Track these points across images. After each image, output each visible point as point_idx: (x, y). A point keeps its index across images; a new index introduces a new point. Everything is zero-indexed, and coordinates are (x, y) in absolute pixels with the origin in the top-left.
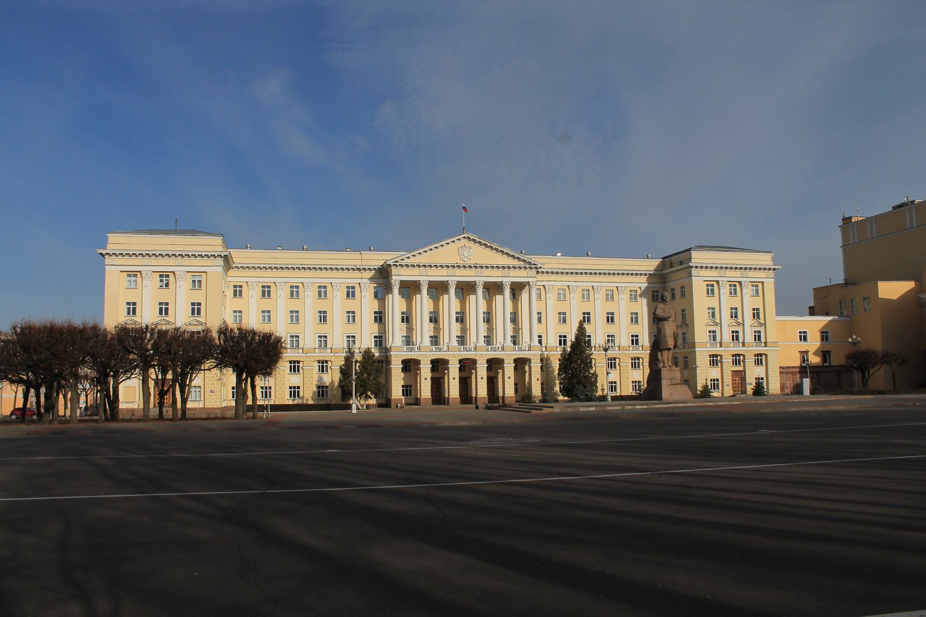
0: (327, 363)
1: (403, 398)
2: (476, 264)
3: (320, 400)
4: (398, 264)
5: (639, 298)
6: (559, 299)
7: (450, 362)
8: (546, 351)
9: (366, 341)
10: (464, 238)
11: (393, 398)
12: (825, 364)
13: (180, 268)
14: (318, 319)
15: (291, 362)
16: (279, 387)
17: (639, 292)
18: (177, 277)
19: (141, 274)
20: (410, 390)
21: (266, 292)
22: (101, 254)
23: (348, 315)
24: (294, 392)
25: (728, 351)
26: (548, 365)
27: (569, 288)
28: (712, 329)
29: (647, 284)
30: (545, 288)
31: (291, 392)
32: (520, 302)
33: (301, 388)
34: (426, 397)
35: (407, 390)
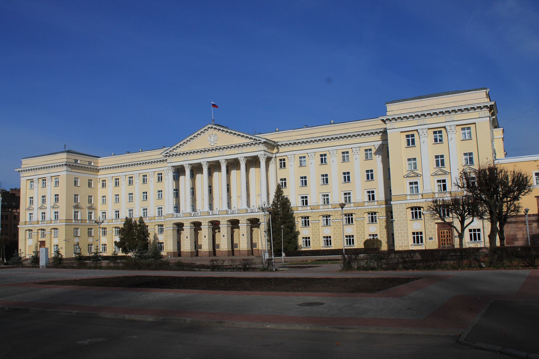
0: (352, 216)
2: (217, 147)
3: (415, 245)
5: (373, 155)
6: (300, 165)
7: (203, 224)
9: (137, 215)
13: (136, 172)
14: (343, 179)
15: (159, 226)
16: (338, 237)
17: (374, 151)
18: (448, 131)
19: (418, 132)
20: (353, 240)
21: (323, 159)
22: (382, 120)
23: (323, 177)
24: (475, 234)
25: (35, 228)
28: (441, 178)
29: (381, 142)
31: (471, 235)
33: (423, 233)
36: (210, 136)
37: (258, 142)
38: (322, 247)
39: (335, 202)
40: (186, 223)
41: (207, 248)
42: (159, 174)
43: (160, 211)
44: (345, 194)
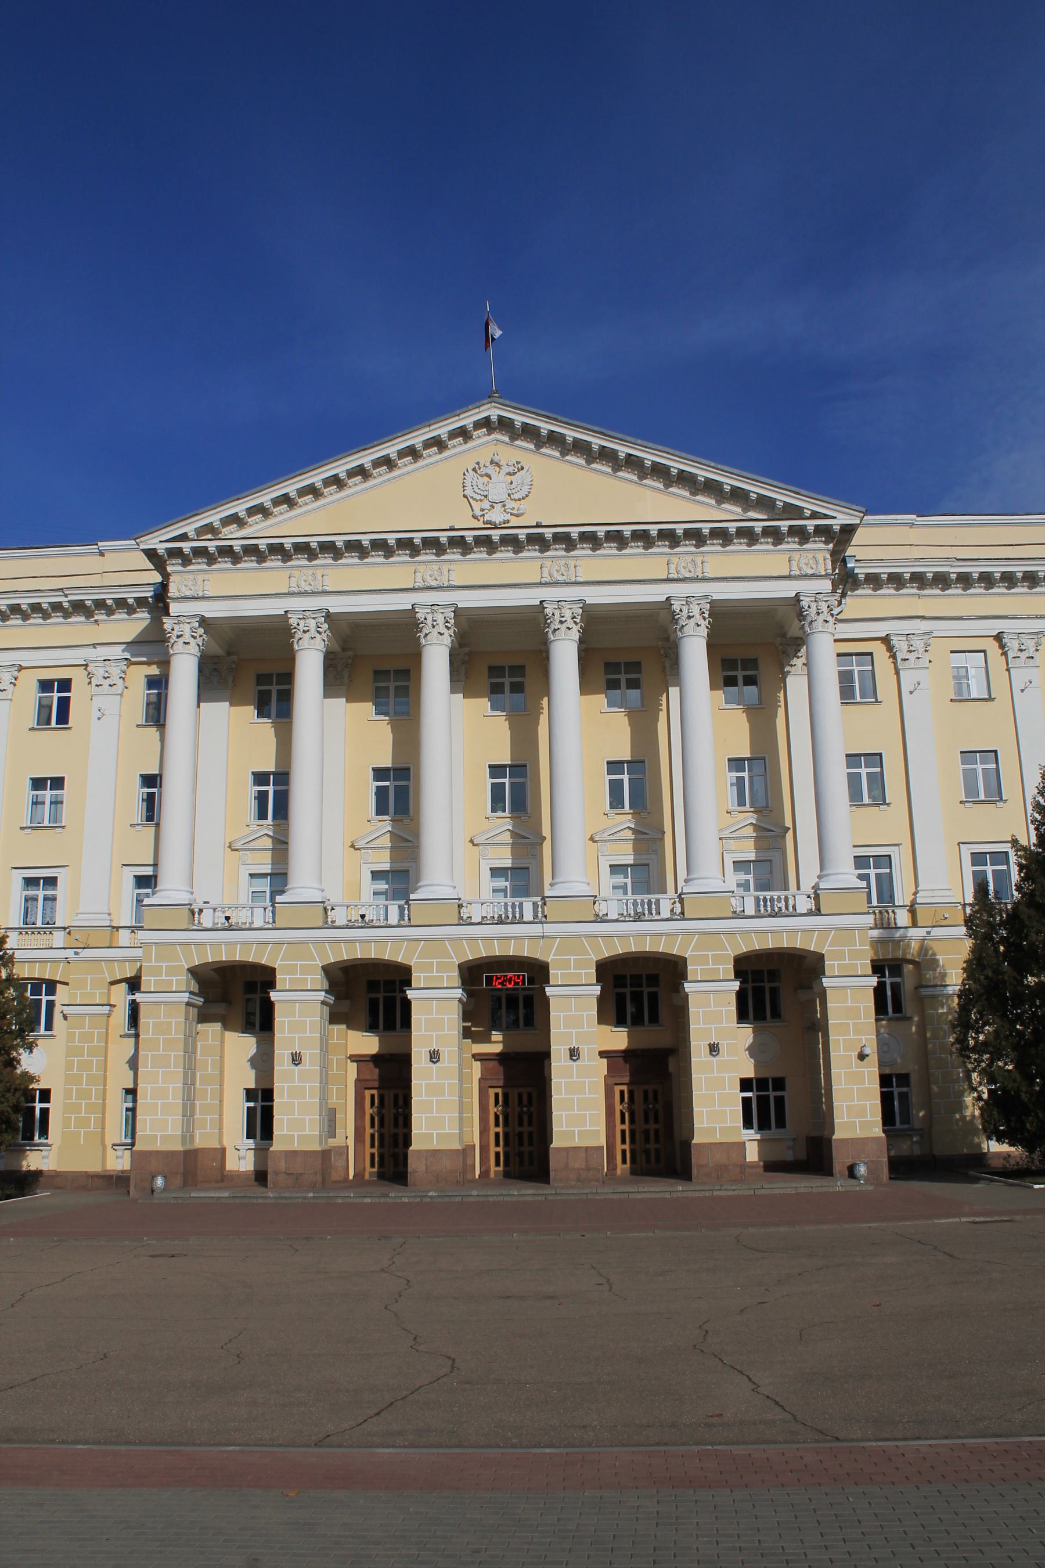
1: (752, 1134)
2: (538, 526)
4: (186, 546)
8: (915, 924)
10: (485, 423)
11: (836, 1136)
12: (402, 922)
20: (780, 1102)
26: (924, 992)
27: (1002, 646)
30: (890, 648)
32: (781, 711)
34: (296, 1146)
35: (763, 1101)
36: (483, 471)
37: (810, 524)
38: (114, 1145)
39: (930, 894)
40: (292, 970)
41: (450, 1128)
42: (46, 685)
43: (35, 899)
44: (30, 882)
